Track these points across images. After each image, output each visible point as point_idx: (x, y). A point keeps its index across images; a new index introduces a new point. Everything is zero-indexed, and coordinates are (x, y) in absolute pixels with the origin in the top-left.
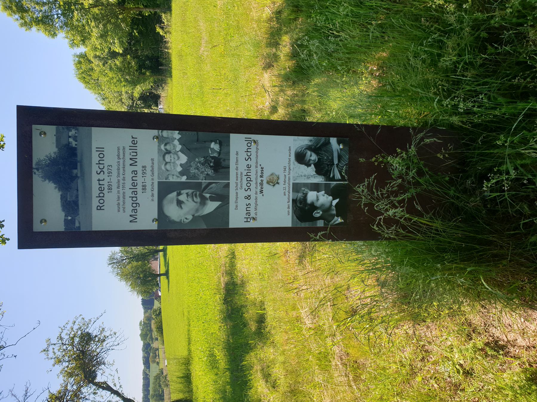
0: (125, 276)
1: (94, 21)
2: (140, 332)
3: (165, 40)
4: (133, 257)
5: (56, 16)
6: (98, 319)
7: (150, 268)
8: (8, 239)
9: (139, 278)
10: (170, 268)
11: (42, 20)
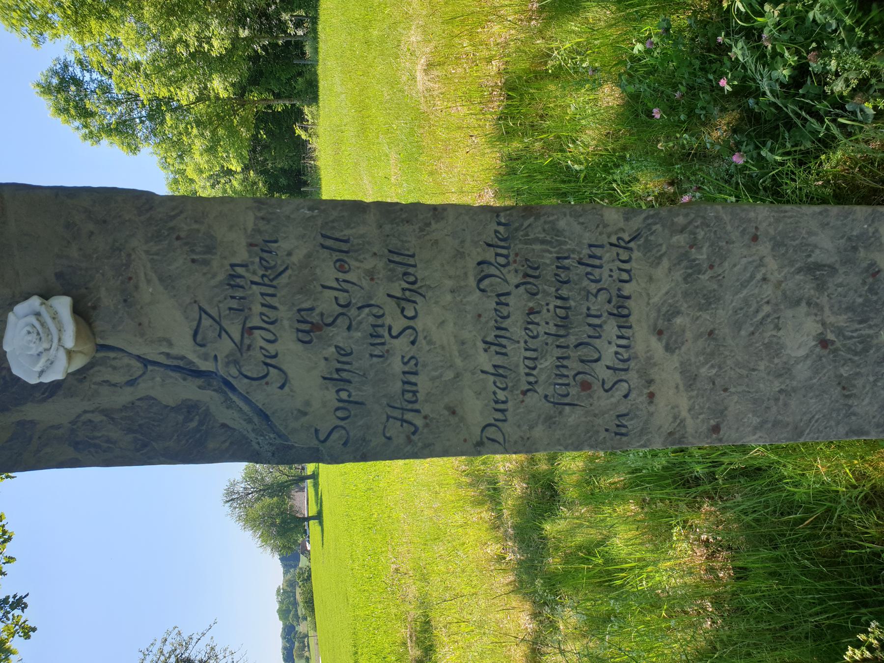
0: (252, 522)
1: (197, 127)
2: (277, 606)
3: (310, 146)
4: (264, 490)
5: (138, 121)
6: (203, 634)
7: (292, 507)
8: (34, 630)
9: (273, 524)
10: (324, 508)
11: (116, 129)
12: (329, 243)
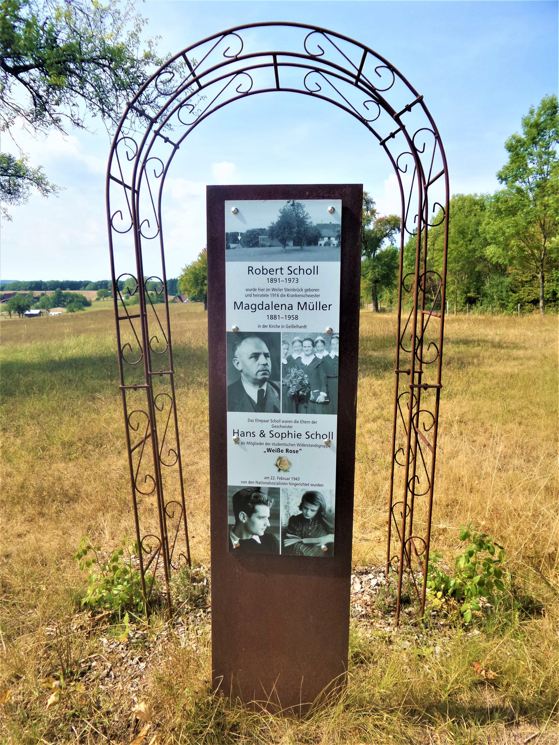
12: (314, 293)
